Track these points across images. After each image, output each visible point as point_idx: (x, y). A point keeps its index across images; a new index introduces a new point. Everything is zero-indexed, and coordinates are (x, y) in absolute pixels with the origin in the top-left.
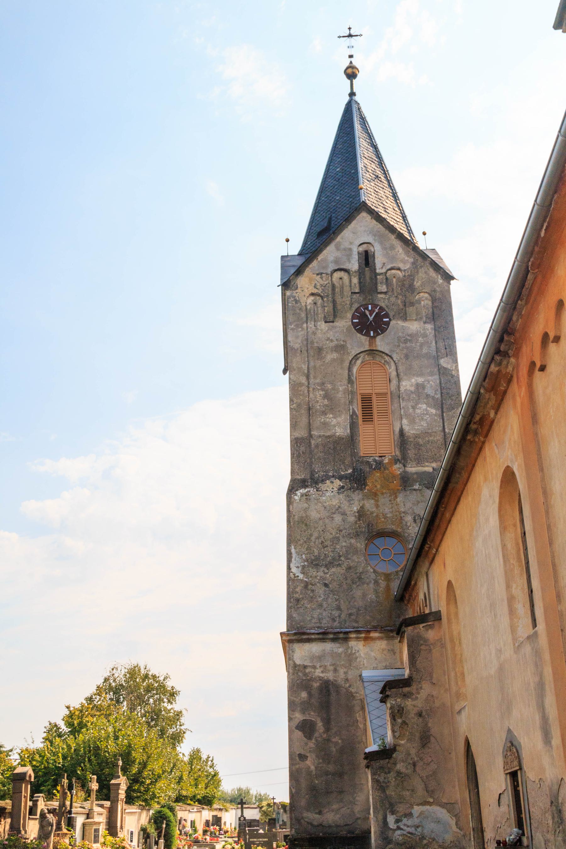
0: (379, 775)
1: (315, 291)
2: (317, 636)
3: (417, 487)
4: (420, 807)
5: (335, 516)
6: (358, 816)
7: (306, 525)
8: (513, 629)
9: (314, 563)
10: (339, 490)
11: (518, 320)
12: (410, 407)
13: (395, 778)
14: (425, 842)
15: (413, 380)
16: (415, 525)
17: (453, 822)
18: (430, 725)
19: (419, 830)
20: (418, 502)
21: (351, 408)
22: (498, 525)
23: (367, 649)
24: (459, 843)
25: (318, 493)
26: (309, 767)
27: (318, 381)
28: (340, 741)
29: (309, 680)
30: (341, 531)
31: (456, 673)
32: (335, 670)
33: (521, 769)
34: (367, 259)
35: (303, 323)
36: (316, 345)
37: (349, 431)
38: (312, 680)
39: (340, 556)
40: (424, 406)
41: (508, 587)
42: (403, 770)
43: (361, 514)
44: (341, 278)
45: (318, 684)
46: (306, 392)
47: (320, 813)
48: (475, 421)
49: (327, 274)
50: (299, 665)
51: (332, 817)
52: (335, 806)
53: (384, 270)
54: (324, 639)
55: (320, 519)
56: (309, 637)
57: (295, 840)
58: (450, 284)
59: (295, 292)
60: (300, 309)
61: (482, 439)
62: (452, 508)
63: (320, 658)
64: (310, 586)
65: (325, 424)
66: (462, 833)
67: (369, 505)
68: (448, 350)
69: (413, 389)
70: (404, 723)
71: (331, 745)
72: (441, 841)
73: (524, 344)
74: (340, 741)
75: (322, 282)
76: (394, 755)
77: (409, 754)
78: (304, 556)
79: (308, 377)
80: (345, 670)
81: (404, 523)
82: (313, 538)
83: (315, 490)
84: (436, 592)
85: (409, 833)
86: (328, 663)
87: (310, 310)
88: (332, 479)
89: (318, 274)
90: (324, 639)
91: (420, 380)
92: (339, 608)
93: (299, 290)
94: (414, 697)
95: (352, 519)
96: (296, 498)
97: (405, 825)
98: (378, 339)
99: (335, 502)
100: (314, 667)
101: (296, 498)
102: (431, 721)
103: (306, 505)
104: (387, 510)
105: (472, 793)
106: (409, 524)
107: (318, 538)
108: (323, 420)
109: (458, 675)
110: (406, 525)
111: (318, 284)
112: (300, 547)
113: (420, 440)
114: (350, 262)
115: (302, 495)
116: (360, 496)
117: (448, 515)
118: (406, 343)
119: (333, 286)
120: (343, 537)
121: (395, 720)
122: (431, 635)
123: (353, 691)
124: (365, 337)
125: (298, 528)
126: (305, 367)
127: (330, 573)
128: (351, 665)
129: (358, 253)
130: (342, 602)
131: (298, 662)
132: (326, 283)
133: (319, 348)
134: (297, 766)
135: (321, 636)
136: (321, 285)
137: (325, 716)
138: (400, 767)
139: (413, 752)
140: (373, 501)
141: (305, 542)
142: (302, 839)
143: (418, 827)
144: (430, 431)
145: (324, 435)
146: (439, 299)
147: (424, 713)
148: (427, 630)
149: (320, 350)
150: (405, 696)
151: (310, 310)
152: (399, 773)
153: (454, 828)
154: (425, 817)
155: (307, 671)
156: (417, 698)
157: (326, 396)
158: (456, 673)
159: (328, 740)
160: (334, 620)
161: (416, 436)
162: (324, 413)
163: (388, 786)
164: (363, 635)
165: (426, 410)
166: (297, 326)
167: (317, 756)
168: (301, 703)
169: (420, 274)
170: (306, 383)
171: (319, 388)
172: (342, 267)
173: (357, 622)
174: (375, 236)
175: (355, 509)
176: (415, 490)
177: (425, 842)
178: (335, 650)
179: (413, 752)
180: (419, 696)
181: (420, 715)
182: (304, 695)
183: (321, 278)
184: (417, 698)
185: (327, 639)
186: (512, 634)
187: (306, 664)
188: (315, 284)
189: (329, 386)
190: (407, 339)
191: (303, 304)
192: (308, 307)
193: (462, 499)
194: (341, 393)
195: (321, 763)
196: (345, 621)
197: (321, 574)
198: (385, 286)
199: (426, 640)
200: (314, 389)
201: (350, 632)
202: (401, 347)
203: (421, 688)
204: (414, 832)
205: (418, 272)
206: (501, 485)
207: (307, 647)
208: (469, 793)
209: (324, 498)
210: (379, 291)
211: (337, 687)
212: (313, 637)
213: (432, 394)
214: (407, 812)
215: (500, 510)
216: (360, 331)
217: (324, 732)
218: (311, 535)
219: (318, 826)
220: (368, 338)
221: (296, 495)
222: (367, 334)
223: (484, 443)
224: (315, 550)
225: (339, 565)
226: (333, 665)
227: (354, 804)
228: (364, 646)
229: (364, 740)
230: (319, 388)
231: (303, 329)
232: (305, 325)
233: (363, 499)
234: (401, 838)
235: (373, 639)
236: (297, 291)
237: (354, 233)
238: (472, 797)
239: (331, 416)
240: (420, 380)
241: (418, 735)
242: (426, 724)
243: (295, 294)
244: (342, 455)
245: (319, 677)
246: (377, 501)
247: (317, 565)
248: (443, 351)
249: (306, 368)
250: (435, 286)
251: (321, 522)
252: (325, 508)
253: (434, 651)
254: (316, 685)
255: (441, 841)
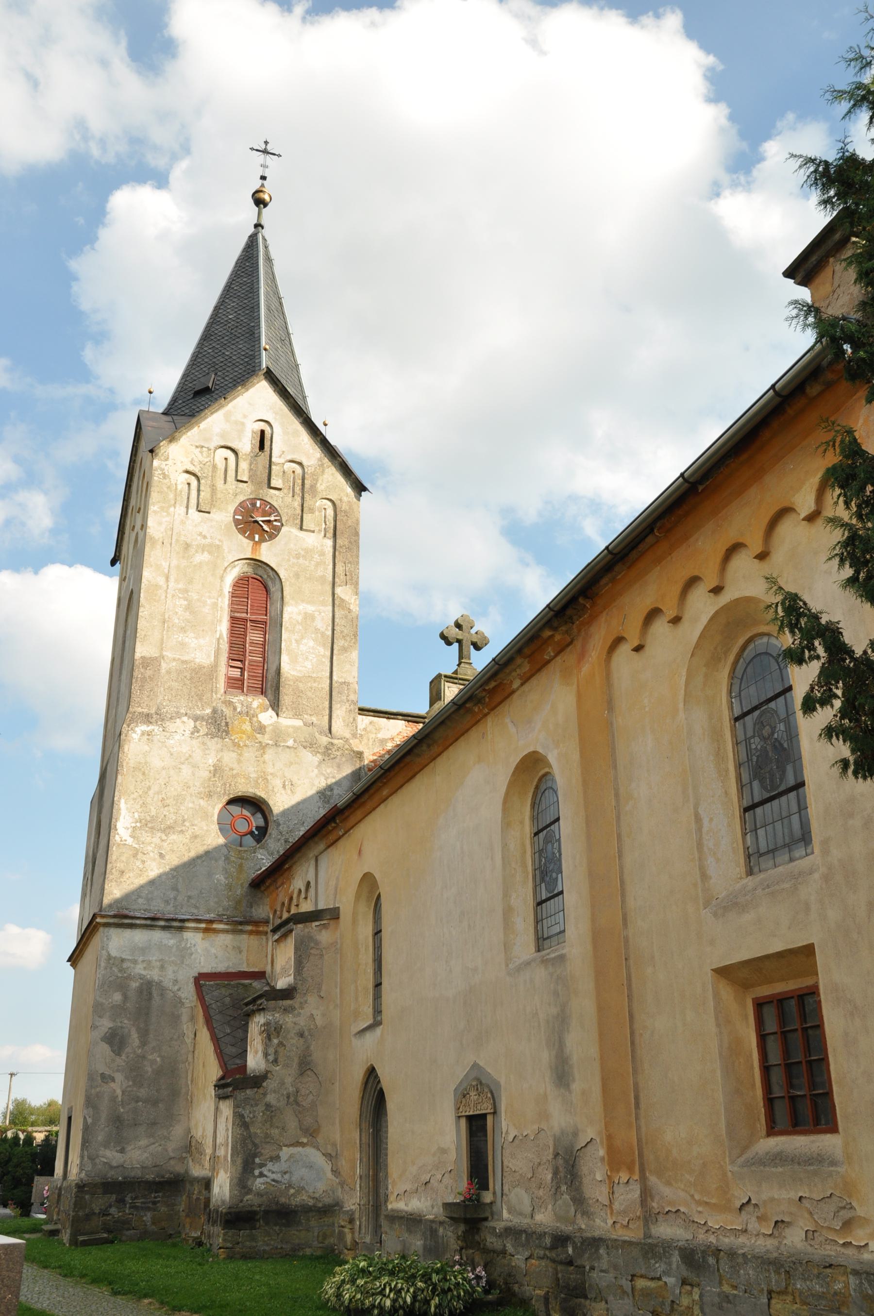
0: (244, 1109)
1: (191, 468)
2: (111, 921)
3: (290, 743)
4: (291, 1148)
5: (183, 767)
6: (172, 1155)
7: (144, 774)
8: (507, 947)
9: (150, 825)
10: (192, 733)
11: (607, 584)
12: (293, 641)
13: (263, 1112)
14: (292, 1191)
15: (301, 607)
16: (283, 792)
17: (327, 1168)
18: (312, 1048)
19: (287, 1176)
20: (291, 763)
21: (218, 628)
22: (500, 820)
23: (207, 944)
24: (333, 1193)
25: (165, 733)
26: (114, 1091)
27: (181, 586)
28: (158, 1059)
29: (126, 978)
30: (189, 787)
31: (357, 988)
32: (162, 968)
33: (494, 1113)
34: (262, 441)
35: (170, 506)
36: (183, 538)
37: (212, 659)
38: (129, 978)
39: (184, 821)
40: (311, 643)
41: (506, 895)
42: (274, 1102)
43: (217, 770)
44: (226, 459)
45: (137, 984)
46: (163, 597)
47: (122, 1151)
48: (487, 688)
49: (209, 449)
50: (115, 958)
51: (138, 1156)
52: (143, 1142)
53: (282, 461)
54: (152, 926)
55: (164, 768)
56: (134, 921)
57: (84, 1186)
58: (361, 496)
59: (164, 463)
60: (168, 487)
61: (486, 710)
62: (769, 837)
63: (144, 950)
64: (140, 855)
65: (183, 645)
66: (337, 1180)
67: (229, 758)
68: (348, 578)
69: (300, 618)
70: (281, 1044)
71: (146, 1063)
72: (311, 1191)
73: (604, 613)
74: (158, 1059)
75: (201, 459)
76: (265, 1084)
77: (284, 1084)
78: (136, 815)
79: (167, 579)
80: (176, 968)
81: (270, 788)
82: (151, 793)
83: (161, 729)
84: (332, 883)
85: (273, 1180)
86: (154, 958)
87: (181, 491)
88: (185, 719)
89: (197, 447)
90: (152, 926)
91: (310, 608)
92: (175, 888)
93: (170, 462)
94: (296, 1012)
95: (205, 774)
96: (134, 735)
97: (269, 1170)
98: (264, 545)
99: (185, 749)
100: (135, 962)
101: (134, 735)
102: (314, 1043)
103: (147, 748)
104: (251, 769)
105: (363, 1135)
106: (276, 790)
107: (158, 793)
108: (180, 639)
109: (360, 989)
110: (273, 791)
111: (196, 460)
112: (132, 802)
113: (301, 685)
114: (240, 441)
115: (143, 734)
116: (219, 746)
117: (385, 792)
118: (298, 558)
119: (214, 467)
120: (191, 795)
121: (270, 1039)
122: (325, 937)
123: (183, 996)
124: (247, 541)
125: (133, 776)
126: (165, 565)
127: (168, 841)
128: (183, 963)
129: (253, 432)
130: (180, 879)
131: (114, 953)
132: (206, 460)
133: (187, 544)
134: (98, 1089)
135: (149, 922)
136: (200, 462)
137: (142, 1025)
138: (271, 1098)
139: (289, 1080)
140: (234, 755)
141: (140, 796)
142: (95, 1185)
143: (285, 1173)
144: (314, 675)
145: (179, 659)
146: (345, 512)
147: (306, 1033)
148: (320, 931)
149: (187, 546)
150: (286, 1010)
151: (181, 491)
152: (268, 1106)
153: (329, 1175)
154: (295, 1161)
155: (125, 965)
156: (299, 1014)
157: (188, 608)
158: (357, 988)
159: (144, 1057)
160: (167, 902)
161: (298, 680)
162: (183, 630)
163: (253, 1122)
164: (203, 925)
165: (313, 648)
166: (162, 508)
167: (127, 1078)
168: (112, 1007)
169: (325, 476)
170: (165, 586)
171: (180, 595)
172: (230, 445)
173: (196, 907)
174: (276, 414)
175: (210, 762)
176: (288, 747)
177: (292, 1191)
178: (165, 941)
179: (289, 1080)
180: (302, 1011)
181: (301, 1035)
182: (117, 997)
183: (201, 452)
184: (299, 1014)
185: (156, 926)
186: (506, 953)
187: (124, 957)
188: (192, 459)
189: (195, 596)
190: (299, 554)
191: (173, 482)
192: (179, 487)
193: (418, 776)
194: (208, 607)
195: (130, 1086)
196: (182, 906)
197: (156, 840)
198: (280, 481)
199: (317, 943)
200: (173, 596)
201: (188, 920)
202: (291, 563)
203: (306, 1002)
204: (280, 1179)
205: (323, 472)
206: (514, 772)
207: (128, 933)
208: (360, 1135)
209: (172, 742)
210: (272, 485)
211: (163, 990)
212: (138, 922)
213: (323, 630)
214: (274, 1154)
215: (505, 801)
216: (242, 532)
217: (139, 1047)
218: (149, 788)
219: (118, 1167)
220: (252, 543)
221: (135, 732)
222: (251, 538)
223: (486, 715)
224: (153, 809)
225: (182, 832)
226: (160, 961)
227: (169, 1139)
228: (203, 939)
229: (190, 1059)
230: (180, 595)
231: (169, 514)
232: (172, 509)
233: (222, 750)
234: (263, 1187)
235: (215, 931)
236: (167, 462)
237: (250, 404)
238: (363, 1139)
239: (192, 635)
240: (310, 608)
241: (296, 1060)
242: (308, 1047)
243: (163, 466)
244: (200, 688)
245: (140, 975)
246: (240, 755)
247: (152, 828)
248: (342, 577)
249: (167, 567)
250: (342, 494)
251: (164, 772)
252: (172, 754)
253: (326, 957)
254: (134, 985)
255: (311, 1191)
